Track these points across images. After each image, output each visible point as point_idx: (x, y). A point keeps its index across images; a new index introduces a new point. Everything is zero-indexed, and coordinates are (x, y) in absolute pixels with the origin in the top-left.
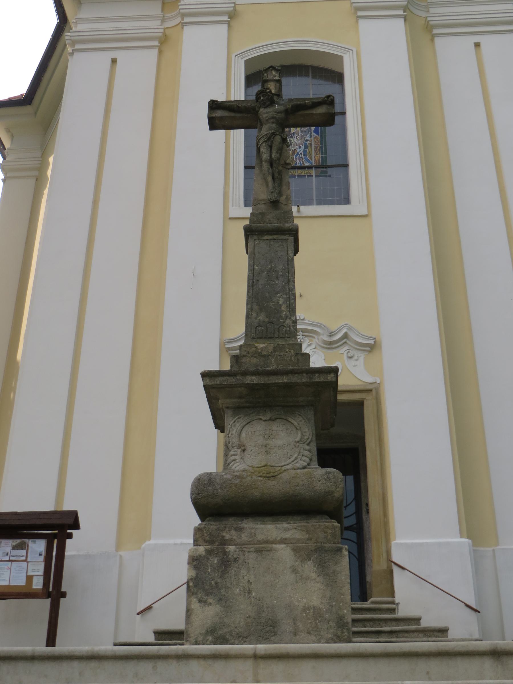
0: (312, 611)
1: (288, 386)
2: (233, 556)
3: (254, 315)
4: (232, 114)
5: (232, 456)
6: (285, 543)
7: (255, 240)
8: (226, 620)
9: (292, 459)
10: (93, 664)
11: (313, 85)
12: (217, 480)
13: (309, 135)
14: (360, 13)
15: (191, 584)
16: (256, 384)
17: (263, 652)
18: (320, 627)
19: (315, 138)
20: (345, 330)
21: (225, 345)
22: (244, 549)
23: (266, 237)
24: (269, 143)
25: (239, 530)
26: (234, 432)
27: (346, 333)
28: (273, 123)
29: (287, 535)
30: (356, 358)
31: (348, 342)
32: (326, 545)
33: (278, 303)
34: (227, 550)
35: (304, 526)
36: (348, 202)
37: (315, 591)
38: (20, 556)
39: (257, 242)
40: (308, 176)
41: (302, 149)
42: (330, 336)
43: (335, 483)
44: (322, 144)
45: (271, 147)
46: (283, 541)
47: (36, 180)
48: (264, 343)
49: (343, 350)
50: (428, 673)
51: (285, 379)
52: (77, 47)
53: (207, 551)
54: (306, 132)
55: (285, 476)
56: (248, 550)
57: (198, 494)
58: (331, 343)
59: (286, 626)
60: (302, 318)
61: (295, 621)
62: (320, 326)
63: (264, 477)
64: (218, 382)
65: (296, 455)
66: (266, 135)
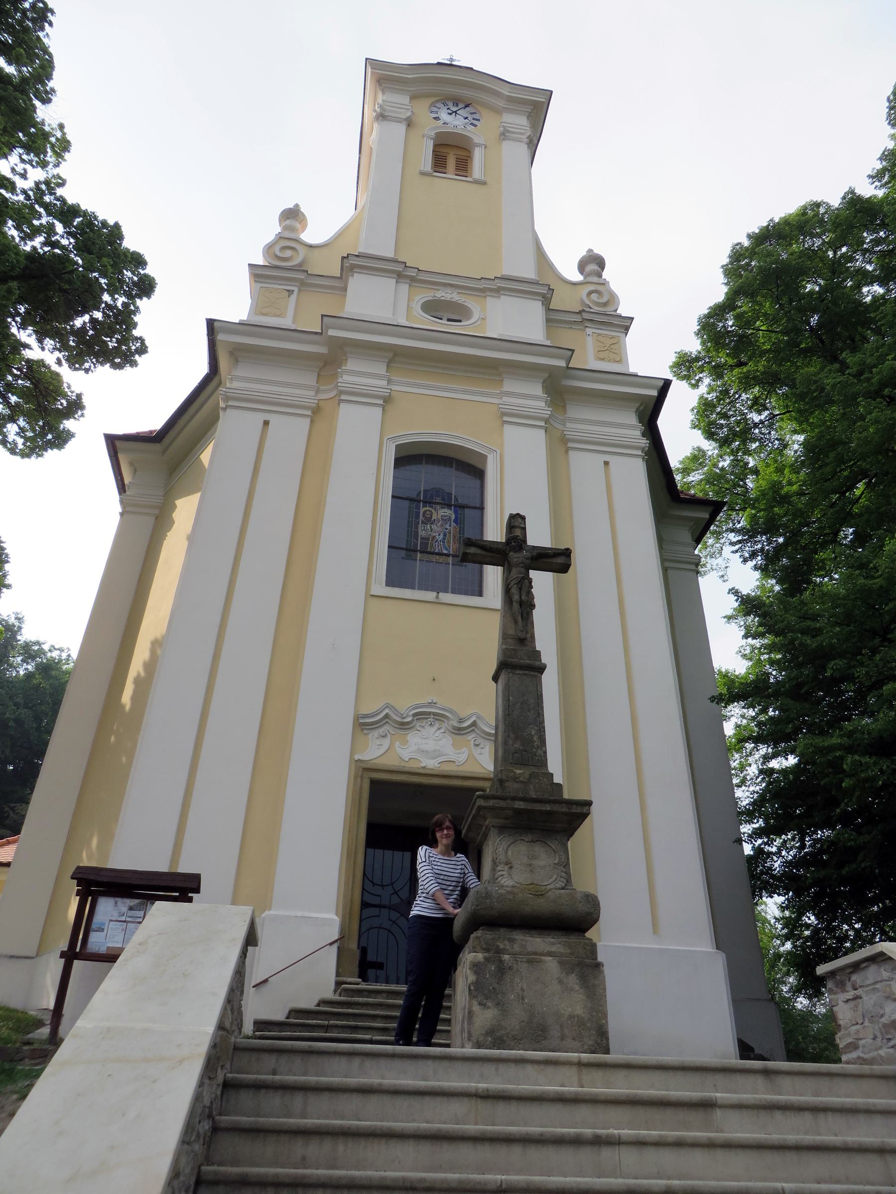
0: (576, 1019)
1: (549, 813)
2: (508, 964)
3: (511, 742)
4: (484, 553)
5: (499, 871)
7: (509, 673)
8: (503, 1023)
9: (552, 880)
10: (445, 1064)
11: (456, 477)
12: (493, 894)
13: (448, 524)
14: (505, 419)
15: (472, 988)
16: (523, 809)
17: (586, 1061)
18: (583, 1034)
19: (454, 527)
20: (473, 719)
21: (358, 720)
22: (518, 959)
23: (518, 672)
24: (520, 586)
25: (512, 941)
26: (501, 849)
27: (475, 722)
28: (522, 567)
29: (553, 949)
30: (482, 746)
31: (475, 730)
32: (587, 960)
34: (503, 959)
35: (566, 941)
36: (480, 594)
37: (578, 1002)
38: (137, 917)
39: (511, 675)
40: (445, 563)
41: (442, 536)
42: (460, 722)
43: (593, 905)
45: (520, 589)
46: (550, 954)
47: (156, 519)
48: (520, 770)
49: (471, 737)
50: (715, 1085)
51: (548, 807)
52: (230, 403)
53: (485, 958)
56: (520, 960)
57: (478, 906)
58: (460, 729)
59: (555, 1032)
60: (435, 702)
61: (561, 1026)
62: (451, 711)
63: (535, 895)
64: (491, 804)
65: (555, 876)
66: (517, 578)
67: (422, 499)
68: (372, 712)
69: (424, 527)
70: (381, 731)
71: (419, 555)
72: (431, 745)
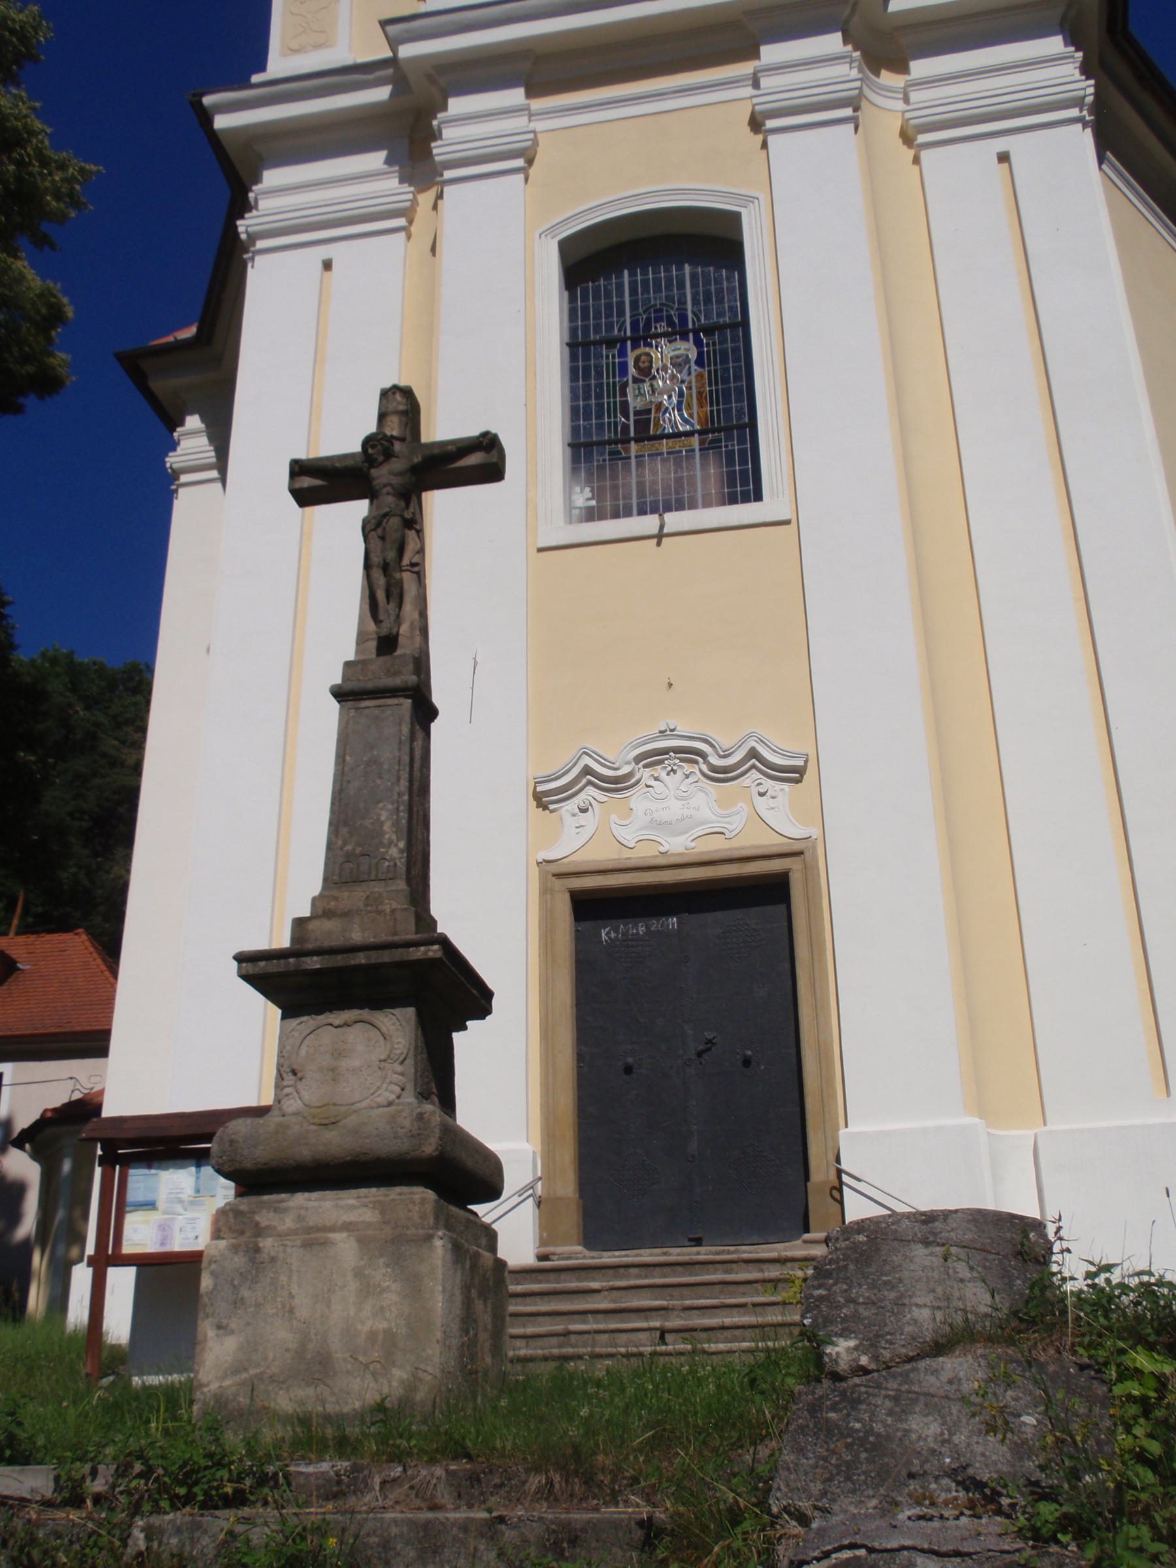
6: (348, 1231)
13: (685, 371)
22: (286, 1242)
33: (378, 819)
34: (261, 1245)
36: (758, 497)
39: (352, 713)
41: (674, 400)
44: (710, 385)
54: (680, 365)
55: (352, 1121)
60: (672, 727)
63: (320, 1125)
67: (629, 333)
68: (554, 770)
69: (639, 389)
70: (579, 800)
71: (633, 446)
72: (674, 809)
